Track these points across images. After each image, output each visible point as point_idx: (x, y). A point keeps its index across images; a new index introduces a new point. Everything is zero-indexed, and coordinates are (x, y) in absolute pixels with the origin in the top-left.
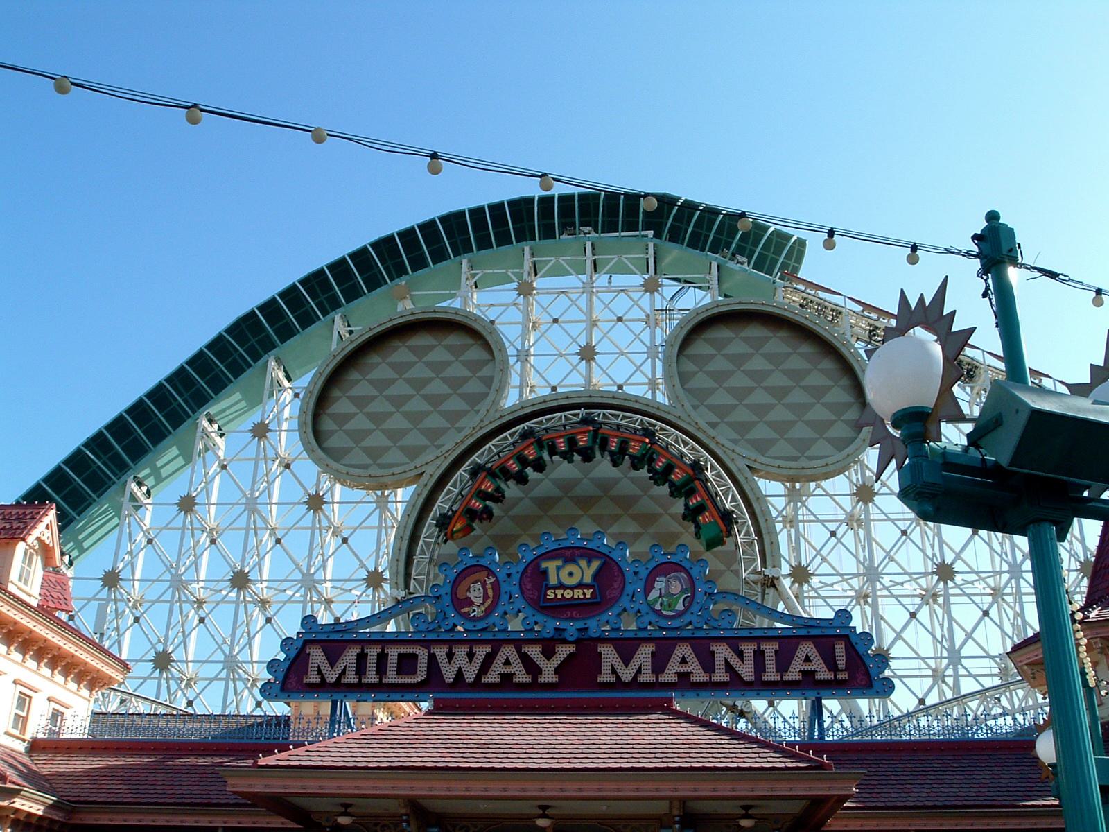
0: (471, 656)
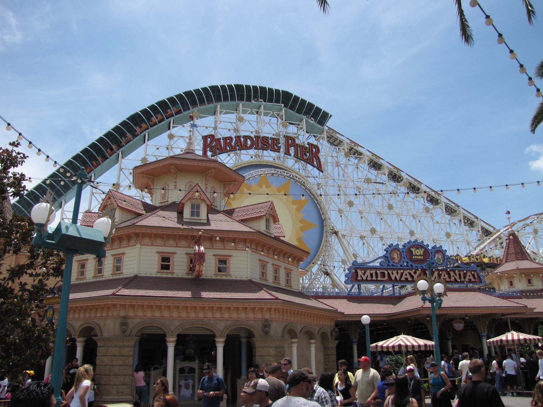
0: (397, 273)
